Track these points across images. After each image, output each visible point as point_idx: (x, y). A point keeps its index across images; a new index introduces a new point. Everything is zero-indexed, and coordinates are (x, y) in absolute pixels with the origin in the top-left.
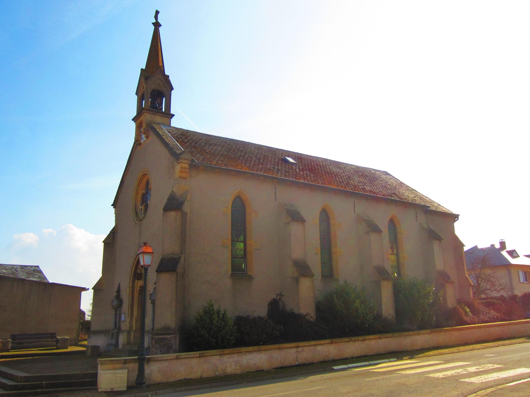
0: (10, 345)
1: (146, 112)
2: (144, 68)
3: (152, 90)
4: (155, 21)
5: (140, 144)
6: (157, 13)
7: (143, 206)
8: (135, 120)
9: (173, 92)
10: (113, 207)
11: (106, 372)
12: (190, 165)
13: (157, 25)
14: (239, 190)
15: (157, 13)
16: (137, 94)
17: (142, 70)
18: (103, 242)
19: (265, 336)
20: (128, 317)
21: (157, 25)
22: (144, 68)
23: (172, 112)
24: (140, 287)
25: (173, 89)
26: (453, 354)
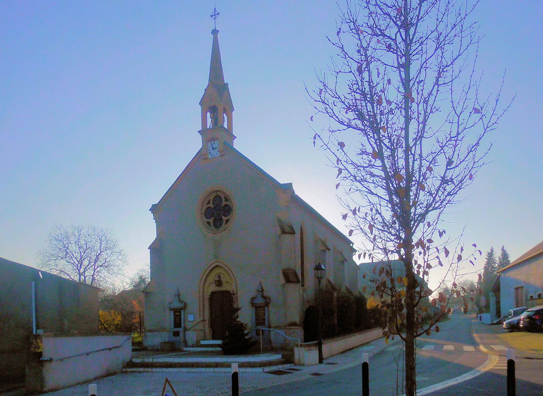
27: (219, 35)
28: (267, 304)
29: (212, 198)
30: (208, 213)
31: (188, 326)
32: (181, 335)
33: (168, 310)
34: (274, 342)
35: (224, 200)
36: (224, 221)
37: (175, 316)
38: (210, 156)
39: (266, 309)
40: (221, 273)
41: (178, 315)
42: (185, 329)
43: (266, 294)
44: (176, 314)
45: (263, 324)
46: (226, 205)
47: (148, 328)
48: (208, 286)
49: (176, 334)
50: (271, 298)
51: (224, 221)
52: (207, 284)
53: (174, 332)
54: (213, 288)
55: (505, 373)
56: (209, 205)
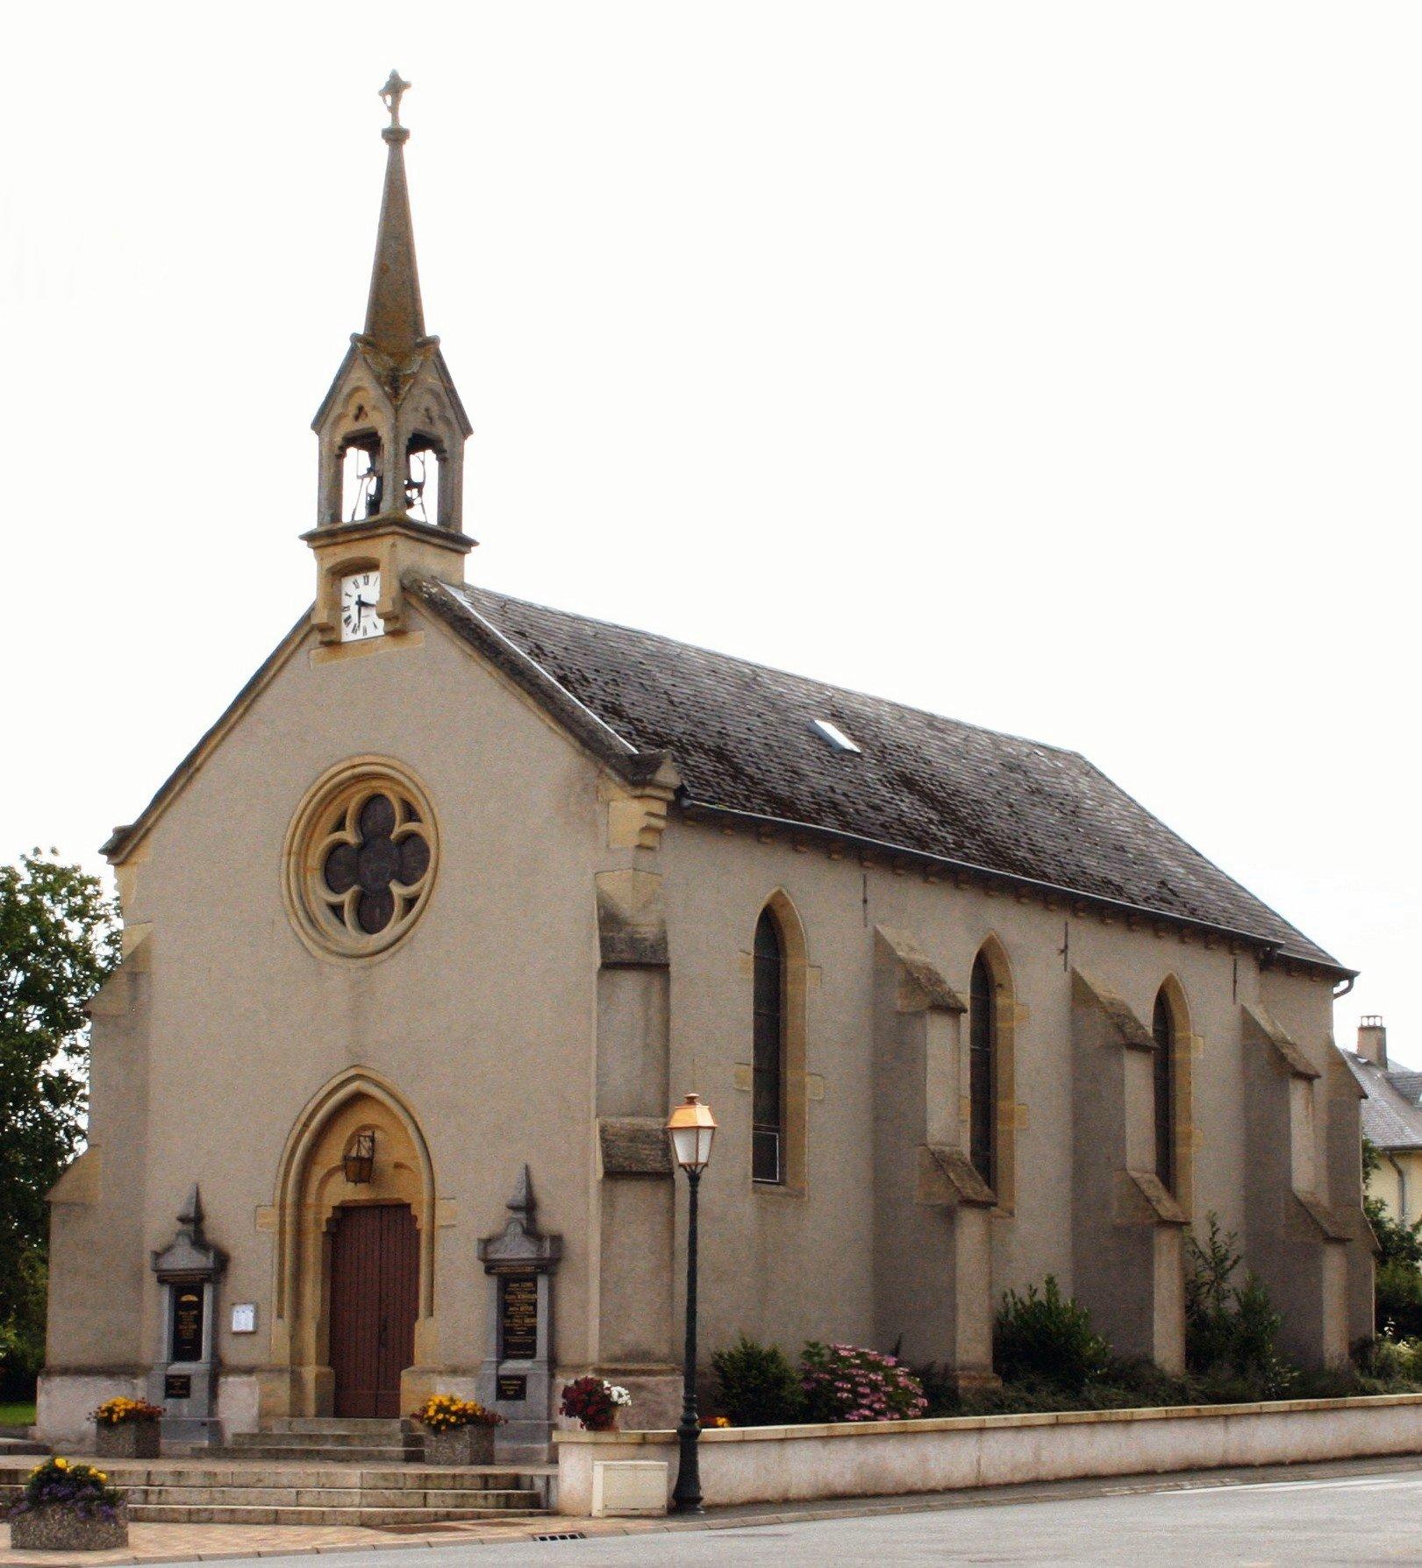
5: (333, 644)
6: (395, 88)
15: (395, 88)
20: (280, 1316)
22: (361, 330)
23: (467, 530)
24: (335, 1208)
27: (408, 149)
28: (549, 1266)
29: (353, 806)
30: (336, 868)
31: (233, 1353)
32: (199, 1387)
33: (150, 1279)
34: (1385, 1352)
35: (398, 815)
36: (398, 906)
37: (178, 1307)
38: (347, 635)
39: (542, 1283)
40: (377, 1127)
41: (190, 1305)
42: (218, 1370)
43: (549, 1221)
44: (184, 1299)
45: (528, 1351)
46: (410, 837)
47: (429, 1364)
48: (324, 1182)
49: (177, 1387)
50: (568, 1237)
51: (398, 906)
52: (318, 1172)
53: (168, 1377)
54: (342, 1191)
55: (965, 1147)
56: (338, 835)
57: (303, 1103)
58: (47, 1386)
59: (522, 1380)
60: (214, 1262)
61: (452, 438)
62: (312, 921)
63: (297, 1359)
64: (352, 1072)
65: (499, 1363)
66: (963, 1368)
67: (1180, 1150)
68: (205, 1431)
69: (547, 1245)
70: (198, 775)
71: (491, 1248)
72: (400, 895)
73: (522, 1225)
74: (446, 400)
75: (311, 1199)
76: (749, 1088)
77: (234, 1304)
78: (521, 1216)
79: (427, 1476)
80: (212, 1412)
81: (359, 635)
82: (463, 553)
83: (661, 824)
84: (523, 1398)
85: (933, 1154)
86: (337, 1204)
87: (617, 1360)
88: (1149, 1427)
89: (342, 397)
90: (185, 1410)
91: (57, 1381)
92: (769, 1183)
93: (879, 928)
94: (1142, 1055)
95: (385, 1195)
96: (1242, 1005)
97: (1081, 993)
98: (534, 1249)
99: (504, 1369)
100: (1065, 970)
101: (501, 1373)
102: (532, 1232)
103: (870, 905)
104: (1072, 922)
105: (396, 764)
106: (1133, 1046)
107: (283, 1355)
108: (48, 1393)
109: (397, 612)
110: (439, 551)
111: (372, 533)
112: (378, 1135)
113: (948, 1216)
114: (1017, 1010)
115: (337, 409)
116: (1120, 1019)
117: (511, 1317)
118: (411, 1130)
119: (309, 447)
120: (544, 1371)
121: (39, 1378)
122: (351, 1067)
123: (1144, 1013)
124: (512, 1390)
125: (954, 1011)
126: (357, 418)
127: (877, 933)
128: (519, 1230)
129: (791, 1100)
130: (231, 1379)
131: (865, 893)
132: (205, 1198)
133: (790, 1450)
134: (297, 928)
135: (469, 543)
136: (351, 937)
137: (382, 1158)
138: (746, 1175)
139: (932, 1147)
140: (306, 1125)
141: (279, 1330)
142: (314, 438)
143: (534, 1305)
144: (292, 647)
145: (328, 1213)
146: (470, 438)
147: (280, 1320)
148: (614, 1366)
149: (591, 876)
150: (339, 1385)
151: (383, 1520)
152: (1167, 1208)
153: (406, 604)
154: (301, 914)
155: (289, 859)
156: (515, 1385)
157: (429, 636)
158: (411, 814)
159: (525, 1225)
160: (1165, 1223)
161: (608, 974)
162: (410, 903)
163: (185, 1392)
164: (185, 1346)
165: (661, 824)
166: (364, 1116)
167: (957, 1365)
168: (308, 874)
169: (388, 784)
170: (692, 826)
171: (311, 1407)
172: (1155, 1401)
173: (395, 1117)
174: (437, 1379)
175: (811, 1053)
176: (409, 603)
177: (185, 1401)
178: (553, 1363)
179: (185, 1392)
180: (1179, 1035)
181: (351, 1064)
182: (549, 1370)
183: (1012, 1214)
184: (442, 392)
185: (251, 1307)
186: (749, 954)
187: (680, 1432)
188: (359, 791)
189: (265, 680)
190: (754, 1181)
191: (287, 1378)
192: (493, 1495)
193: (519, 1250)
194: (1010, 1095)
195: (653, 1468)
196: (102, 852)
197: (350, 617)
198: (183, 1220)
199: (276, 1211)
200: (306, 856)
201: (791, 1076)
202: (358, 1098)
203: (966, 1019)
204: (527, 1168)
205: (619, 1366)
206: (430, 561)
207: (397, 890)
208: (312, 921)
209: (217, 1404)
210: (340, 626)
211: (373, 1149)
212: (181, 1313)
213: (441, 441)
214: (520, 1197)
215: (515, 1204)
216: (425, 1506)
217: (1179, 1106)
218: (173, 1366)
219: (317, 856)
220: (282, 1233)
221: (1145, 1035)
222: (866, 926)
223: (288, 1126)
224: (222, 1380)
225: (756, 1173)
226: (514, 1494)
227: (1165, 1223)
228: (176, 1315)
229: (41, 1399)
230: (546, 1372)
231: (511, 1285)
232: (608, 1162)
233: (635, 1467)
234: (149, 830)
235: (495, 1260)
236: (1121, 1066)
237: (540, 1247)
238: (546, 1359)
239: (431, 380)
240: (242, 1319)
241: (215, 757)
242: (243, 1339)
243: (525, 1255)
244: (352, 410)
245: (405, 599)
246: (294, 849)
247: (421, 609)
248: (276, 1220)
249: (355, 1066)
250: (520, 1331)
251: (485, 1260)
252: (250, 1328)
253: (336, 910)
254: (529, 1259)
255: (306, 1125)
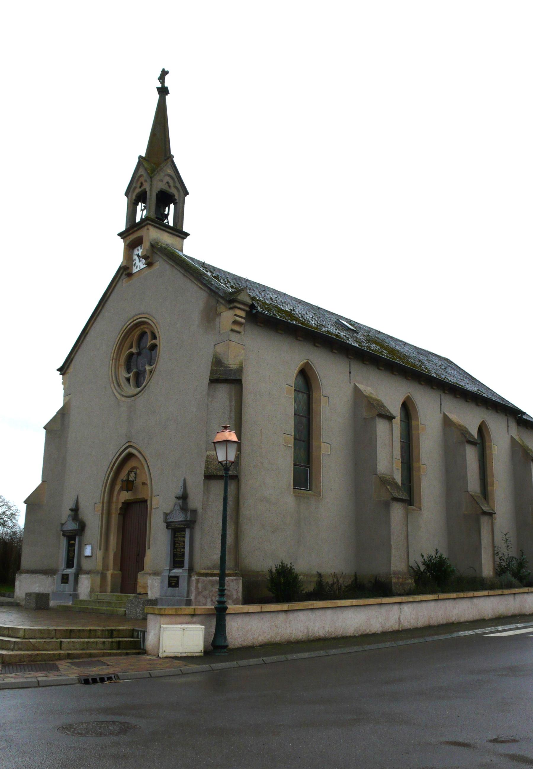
0: (256, 601)
1: (150, 224)
2: (144, 155)
3: (159, 190)
4: (160, 85)
5: (130, 275)
6: (164, 73)
7: (131, 374)
8: (125, 235)
9: (187, 198)
10: (59, 372)
11: (41, 640)
12: (247, 313)
13: (163, 91)
14: (306, 361)
15: (164, 73)
16: (127, 194)
17: (140, 157)
18: (45, 428)
19: (150, 582)
20: (100, 549)
21: (163, 91)
22: (144, 155)
23: (185, 229)
24: (123, 503)
25: (187, 193)
26: (335, 606)
28: (190, 524)
31: (86, 565)
54: (125, 496)
55: (398, 478)
57: (111, 459)
58: (19, 577)
59: (177, 577)
60: (78, 527)
61: (179, 195)
62: (119, 385)
63: (106, 567)
64: (127, 445)
65: (170, 570)
66: (395, 573)
67: (489, 488)
68: (71, 597)
69: (189, 514)
70: (88, 335)
71: (168, 517)
72: (148, 370)
73: (180, 506)
74: (176, 180)
75: (115, 499)
76: (291, 445)
77: (86, 544)
78: (180, 502)
79: (71, 631)
80: (75, 589)
81: (138, 269)
82: (184, 238)
83: (243, 321)
84: (178, 587)
85: (380, 478)
86: (123, 501)
87: (208, 568)
88: (482, 599)
89: (135, 181)
90: (67, 589)
91: (24, 575)
92: (306, 490)
93: (357, 384)
94: (473, 446)
95: (140, 496)
96: (511, 436)
97: (447, 422)
98: (183, 516)
99: (172, 573)
100: (441, 413)
101: (171, 574)
102: (184, 508)
103: (352, 374)
104: (443, 396)
105: (155, 321)
106: (470, 442)
107: (99, 566)
108: (20, 581)
109: (148, 255)
110: (170, 235)
111: (141, 226)
112: (138, 471)
113: (387, 506)
114: (420, 426)
115: (134, 185)
116: (463, 432)
117: (176, 548)
118: (146, 466)
119: (124, 201)
120: (186, 574)
121: (17, 575)
122: (127, 443)
123: (474, 432)
124: (174, 583)
125: (390, 418)
126: (140, 187)
127: (355, 386)
128: (178, 508)
129: (314, 453)
130: (83, 576)
131: (350, 369)
132: (80, 501)
133: (291, 616)
134: (113, 388)
135: (187, 235)
136: (132, 390)
137: (139, 481)
138: (290, 485)
139: (380, 475)
140: (112, 469)
141: (100, 554)
142: (126, 199)
143: (184, 542)
144: (117, 279)
145: (120, 505)
146: (188, 196)
147: (100, 551)
148: (206, 571)
149: (213, 344)
150: (123, 577)
151: (20, 660)
152: (486, 509)
153: (153, 252)
154: (115, 382)
155: (112, 362)
156: (175, 580)
157: (160, 264)
158: (154, 337)
159: (181, 506)
160: (485, 513)
161: (214, 385)
162: (151, 371)
163: (66, 581)
164: (70, 564)
165: (243, 321)
166: (132, 463)
167: (392, 572)
168: (120, 367)
169: (145, 326)
170: (260, 326)
171: (109, 589)
172: (484, 589)
173: (142, 464)
174: (148, 577)
175: (324, 433)
176: (154, 252)
177: (67, 585)
178: (191, 570)
179: (66, 581)
180: (487, 444)
181: (126, 441)
182: (188, 574)
183: (421, 509)
184: (174, 176)
185: (90, 546)
186: (292, 387)
187: (216, 608)
188: (138, 331)
189: (107, 296)
190: (294, 488)
191: (99, 576)
192: (109, 642)
193: (179, 517)
194: (419, 460)
195: (197, 629)
196: (58, 370)
197: (135, 263)
198: (71, 510)
199: (101, 505)
200: (119, 360)
201: (314, 444)
202: (130, 456)
203: (397, 423)
204: (185, 480)
205: (209, 572)
206: (167, 239)
207: (148, 368)
208: (119, 385)
209: (78, 586)
210: (132, 267)
211: (136, 477)
212: (70, 548)
213: (174, 196)
214: (180, 493)
215: (178, 496)
216: (61, 649)
217: (489, 473)
218: (66, 570)
219: (124, 358)
220: (102, 514)
221: (474, 439)
222: (350, 383)
223: (106, 469)
224: (80, 576)
225: (295, 485)
226: (123, 641)
227: (485, 513)
228: (68, 548)
229: (17, 583)
230: (187, 574)
231: (177, 534)
232: (206, 471)
233: (183, 629)
234: (72, 359)
235: (171, 522)
236: (465, 450)
237: (186, 515)
238: (187, 568)
239: (170, 171)
240: (88, 551)
241: (93, 328)
242: (87, 559)
243: (180, 520)
244: (139, 185)
245: (152, 250)
246: (114, 357)
247: (157, 252)
248: (101, 508)
249: (128, 442)
250: (179, 555)
251: (166, 522)
252: (90, 555)
253: (128, 380)
254: (182, 521)
255: (112, 469)
